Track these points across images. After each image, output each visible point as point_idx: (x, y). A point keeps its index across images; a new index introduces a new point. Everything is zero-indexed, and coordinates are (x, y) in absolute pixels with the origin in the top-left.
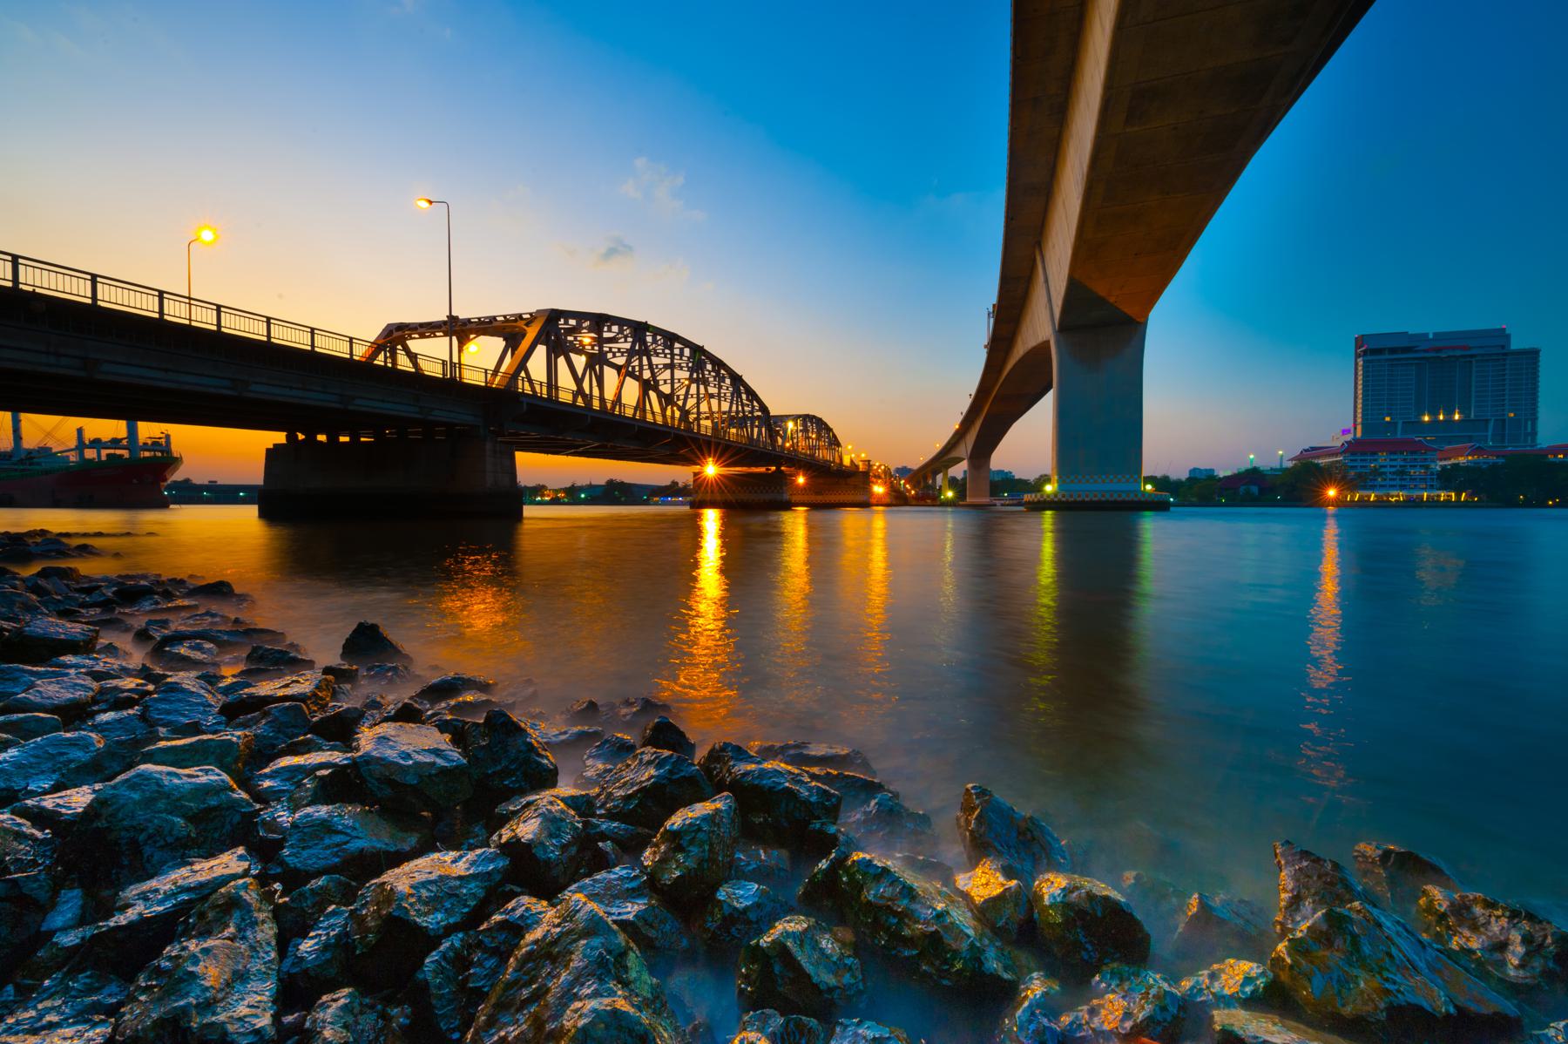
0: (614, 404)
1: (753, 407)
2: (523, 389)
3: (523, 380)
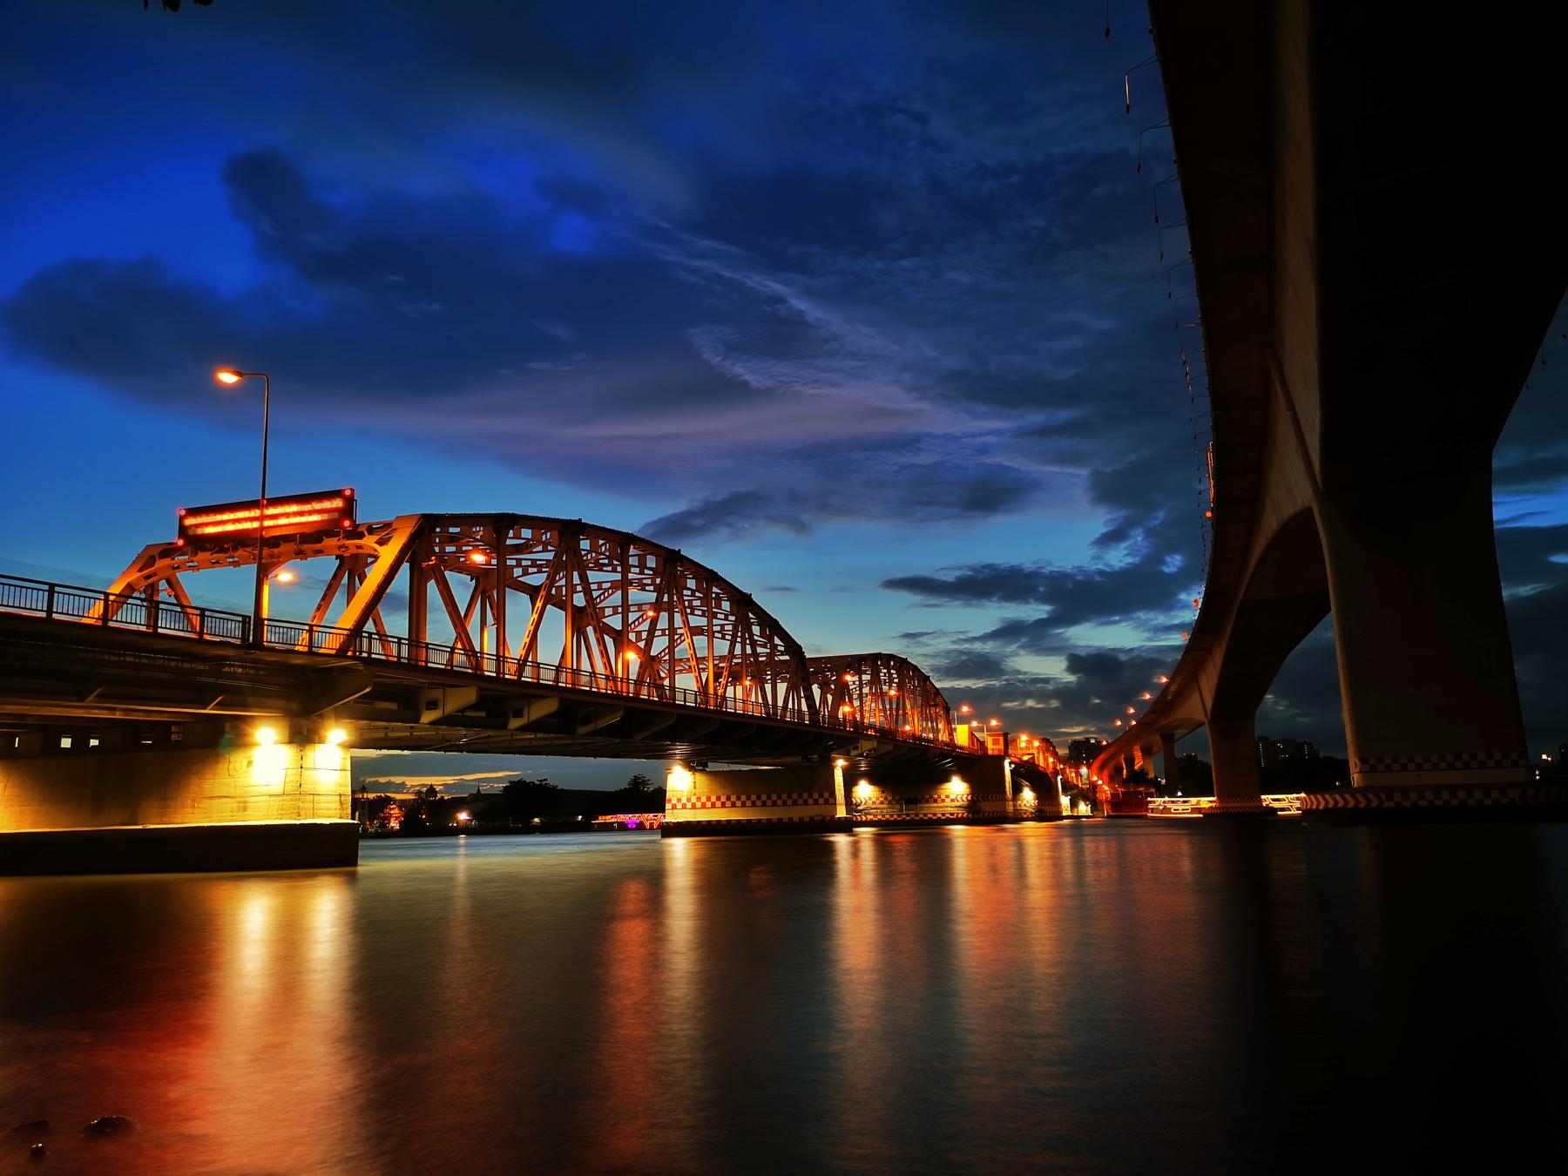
0: (522, 664)
2: (370, 653)
3: (370, 638)
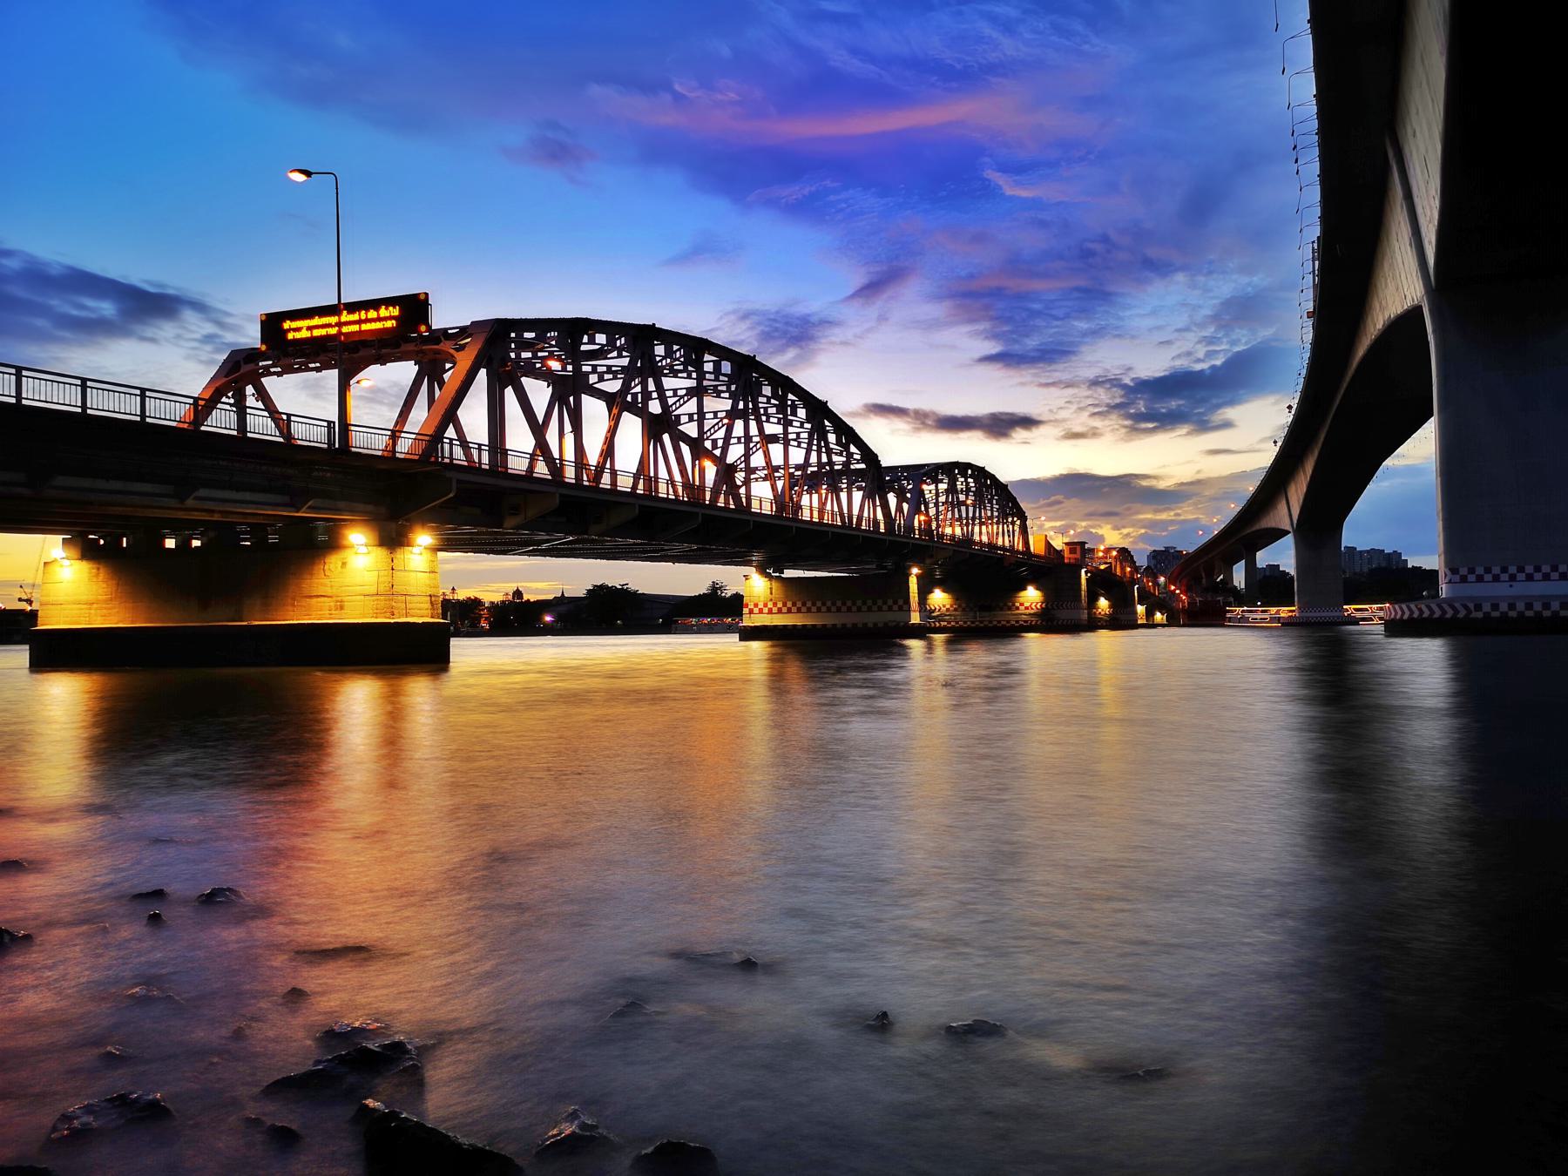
1: (850, 455)
2: (451, 458)
3: (451, 444)
